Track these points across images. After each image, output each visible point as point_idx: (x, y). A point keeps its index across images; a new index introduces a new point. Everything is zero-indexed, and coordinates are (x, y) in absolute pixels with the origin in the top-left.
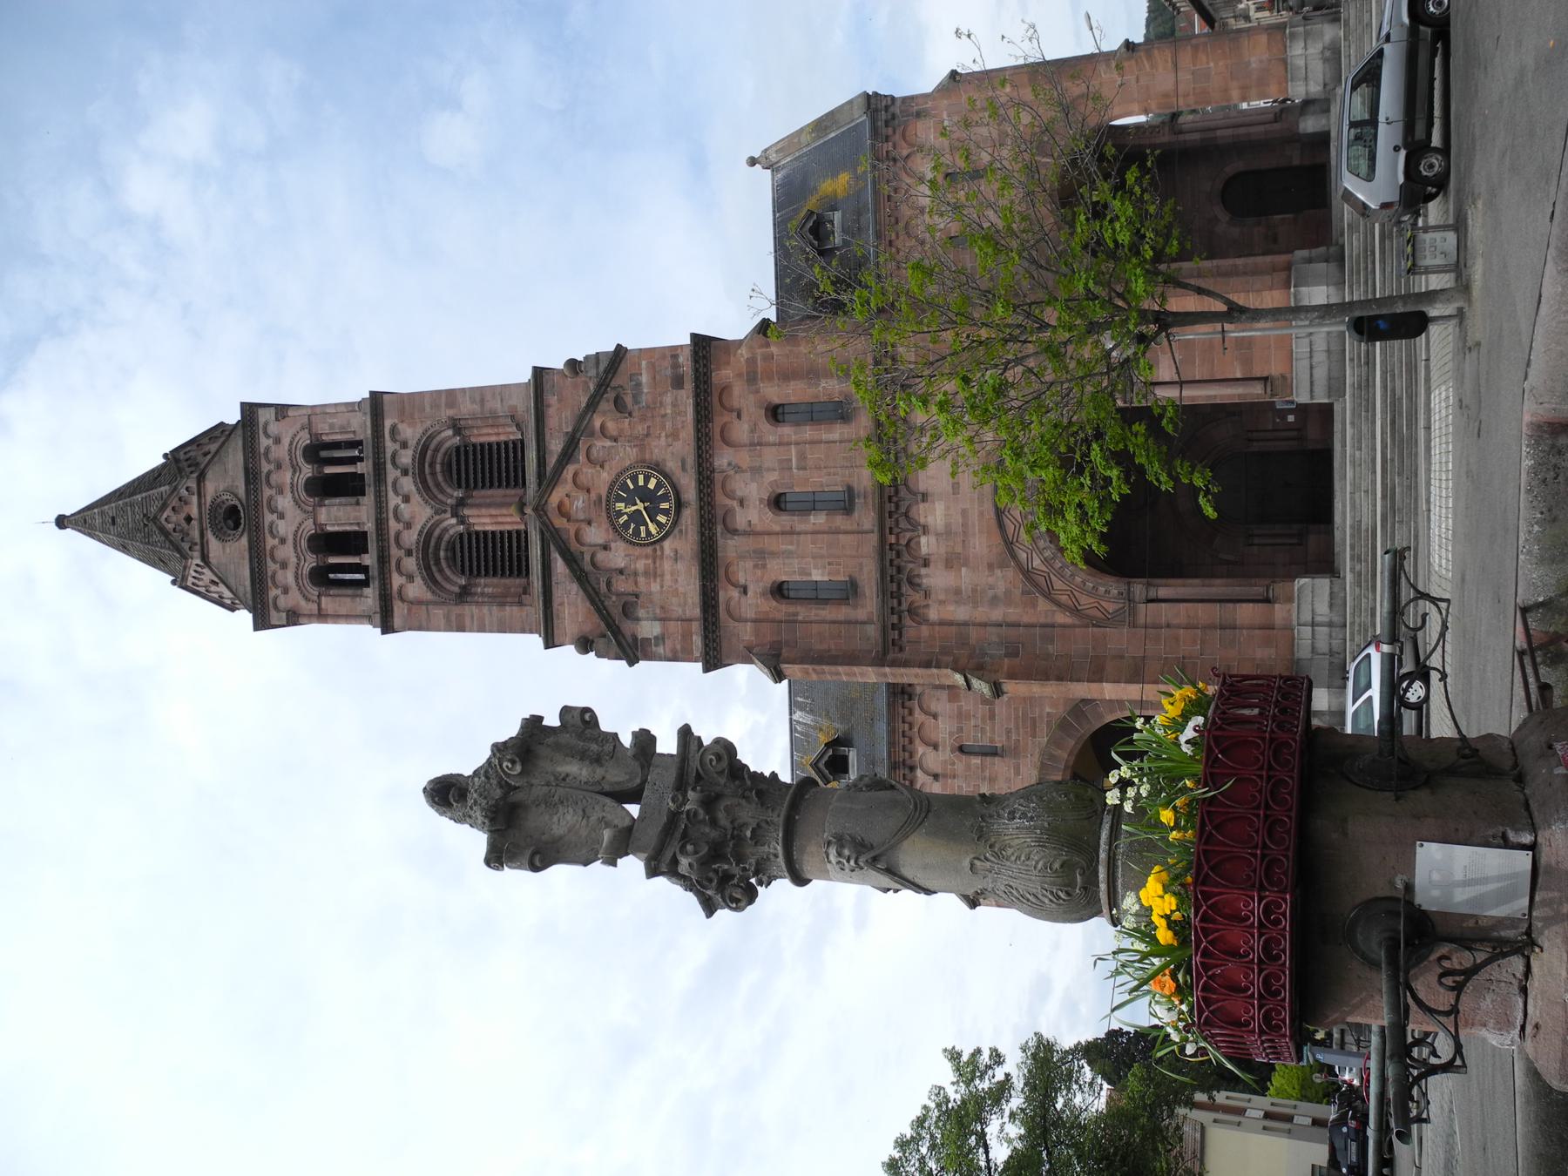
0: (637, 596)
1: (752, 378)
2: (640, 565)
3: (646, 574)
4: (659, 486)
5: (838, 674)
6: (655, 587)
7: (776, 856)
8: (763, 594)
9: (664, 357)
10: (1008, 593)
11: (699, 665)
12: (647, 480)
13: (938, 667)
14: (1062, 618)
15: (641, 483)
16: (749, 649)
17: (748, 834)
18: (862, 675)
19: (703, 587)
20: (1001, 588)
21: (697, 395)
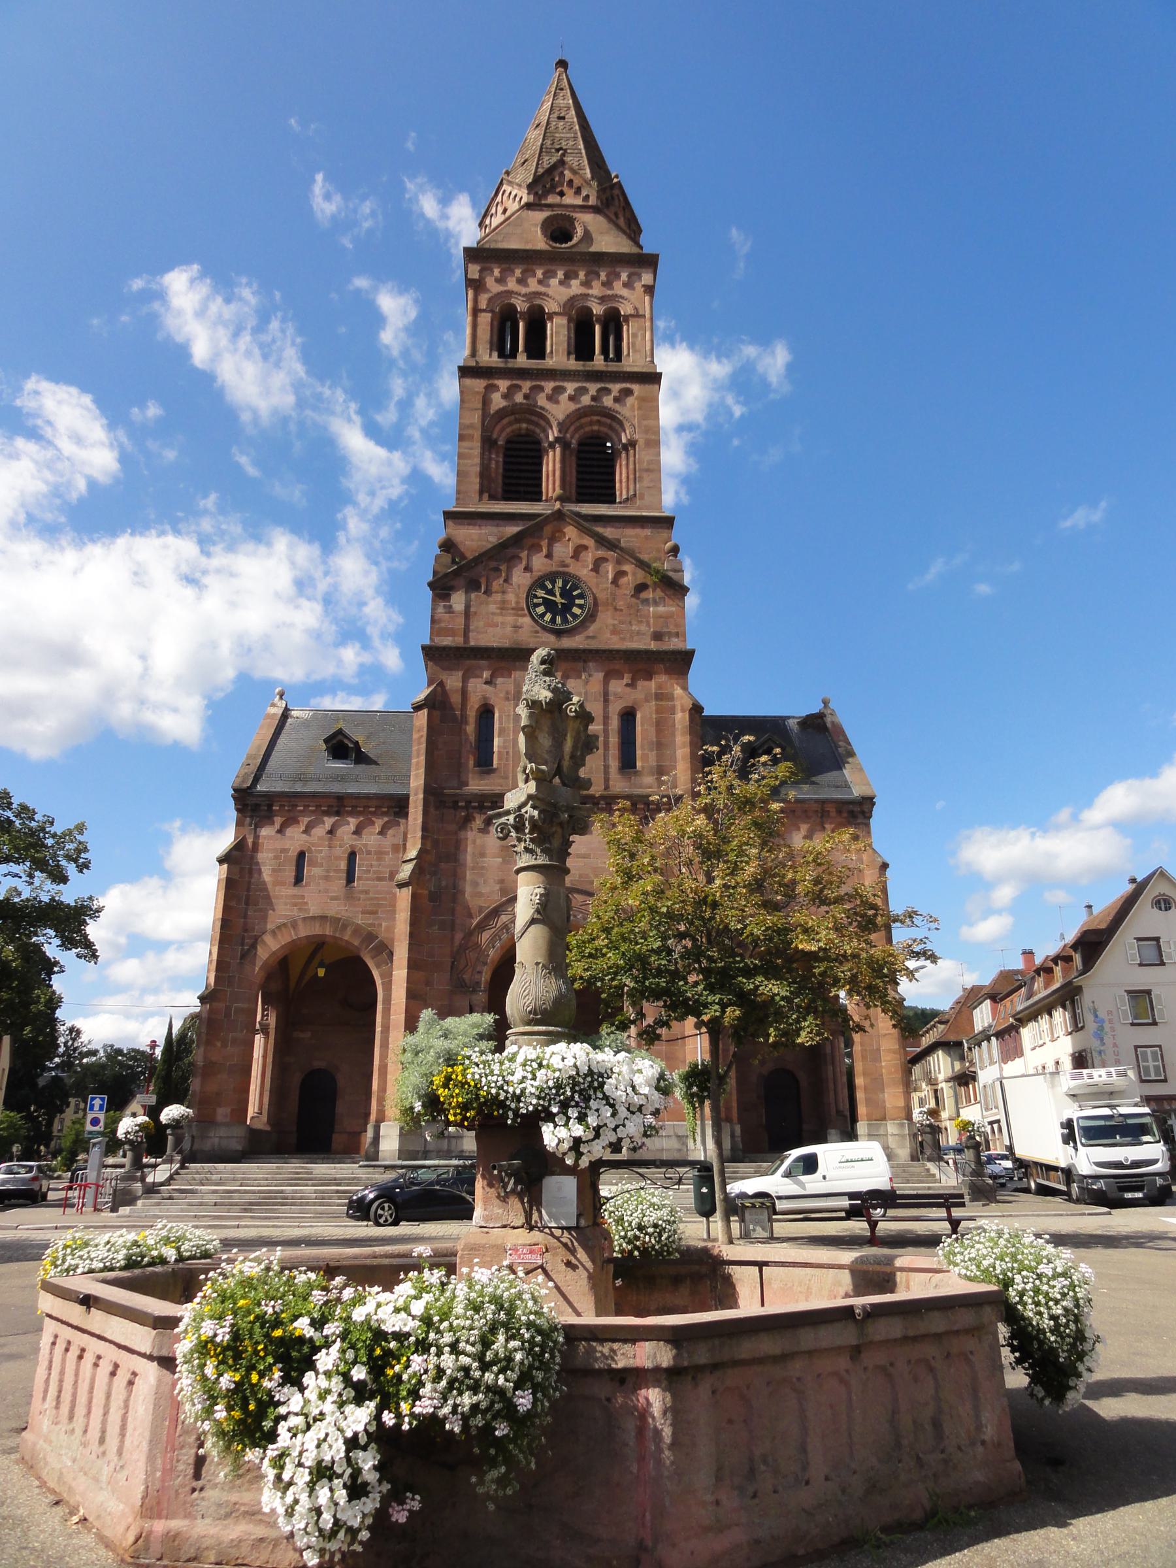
0: (485, 593)
1: (659, 697)
3: (504, 602)
4: (575, 616)
6: (493, 608)
9: (677, 626)
10: (480, 894)
11: (427, 642)
12: (580, 606)
13: (423, 838)
14: (459, 936)
18: (417, 775)
19: (492, 649)
20: (485, 890)
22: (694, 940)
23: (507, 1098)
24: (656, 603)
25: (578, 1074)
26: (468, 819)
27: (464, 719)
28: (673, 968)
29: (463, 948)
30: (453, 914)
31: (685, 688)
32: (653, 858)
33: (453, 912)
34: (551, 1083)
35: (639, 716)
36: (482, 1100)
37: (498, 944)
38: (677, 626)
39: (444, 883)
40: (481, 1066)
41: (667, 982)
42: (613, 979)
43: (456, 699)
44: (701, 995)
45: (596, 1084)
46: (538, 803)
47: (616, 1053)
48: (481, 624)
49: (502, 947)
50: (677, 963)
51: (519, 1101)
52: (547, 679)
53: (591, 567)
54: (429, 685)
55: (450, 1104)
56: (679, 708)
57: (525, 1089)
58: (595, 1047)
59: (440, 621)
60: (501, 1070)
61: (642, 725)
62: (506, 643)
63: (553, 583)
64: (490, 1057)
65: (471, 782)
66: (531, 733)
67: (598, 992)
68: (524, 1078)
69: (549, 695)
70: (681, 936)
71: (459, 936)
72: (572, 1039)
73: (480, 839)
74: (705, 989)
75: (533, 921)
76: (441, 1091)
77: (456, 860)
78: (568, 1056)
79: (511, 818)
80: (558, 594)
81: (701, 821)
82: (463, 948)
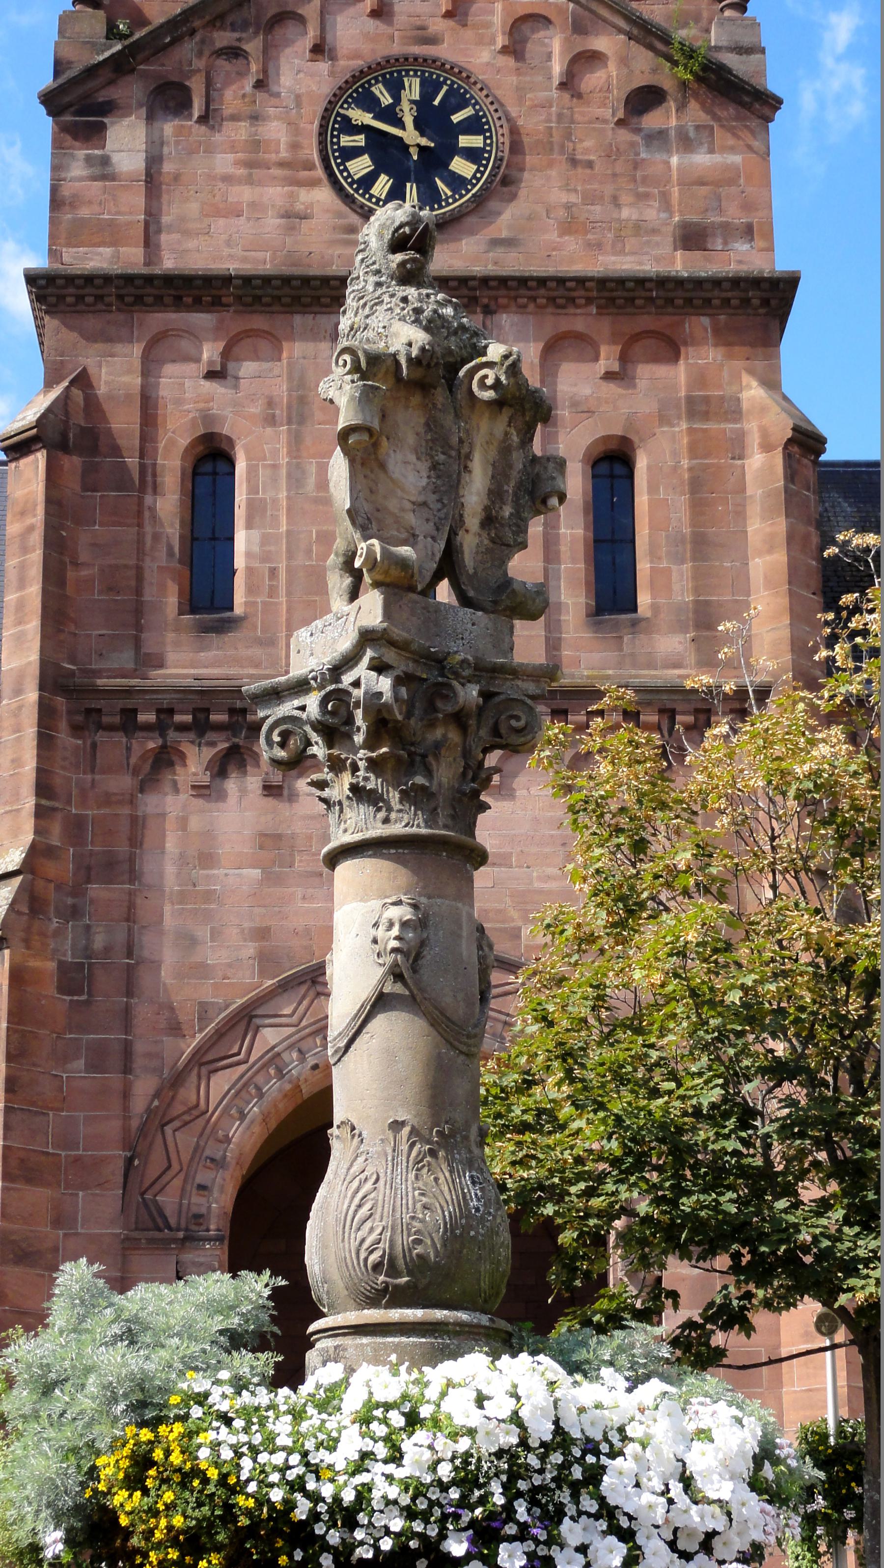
0: (203, 119)
1: (699, 408)
2: (275, 131)
3: (256, 145)
4: (458, 183)
5: (22, 584)
6: (224, 162)
7: (386, 821)
8: (207, 418)
9: (747, 206)
10: (202, 970)
11: (39, 261)
12: (472, 155)
13: (40, 813)
14: (144, 1088)
15: (465, 141)
16: (83, 380)
17: (419, 780)
18: (19, 638)
19: (227, 280)
20: (214, 956)
21: (662, 282)
22: (813, 1082)
23: (315, 1516)
24: (687, 144)
25: (524, 1443)
26: (165, 760)
27: (148, 479)
28: (759, 1162)
29: (158, 1119)
30: (127, 1027)
31: (772, 383)
32: (704, 852)
33: (126, 1017)
34: (445, 1471)
35: (641, 464)
36: (244, 1521)
37: (254, 1110)
38: (747, 206)
39: (99, 941)
40: (239, 1423)
41: (739, 1202)
42: (590, 1193)
43: (124, 423)
44: (837, 1238)
45: (577, 1473)
46: (390, 656)
47: (634, 1383)
48: (193, 208)
49: (265, 1118)
50: (768, 1147)
51: (351, 1524)
52: (411, 292)
53: (500, 41)
54: (49, 384)
55: (149, 1534)
56: (754, 440)
57: (368, 1488)
58: (572, 1368)
59: (74, 202)
60: (297, 1435)
61: (652, 489)
62: (264, 263)
63: (396, 88)
64: (263, 1397)
65: (171, 656)
66: (364, 448)
67: (550, 1229)
68: (365, 1455)
69: (420, 337)
70: (779, 1071)
71: (144, 1088)
72: (504, 1344)
73: (200, 816)
74: (847, 1221)
75: (380, 1002)
76: (120, 1497)
77: (134, 875)
78: (497, 1392)
79: (312, 702)
80: (408, 120)
81: (831, 747)
82: (158, 1119)
